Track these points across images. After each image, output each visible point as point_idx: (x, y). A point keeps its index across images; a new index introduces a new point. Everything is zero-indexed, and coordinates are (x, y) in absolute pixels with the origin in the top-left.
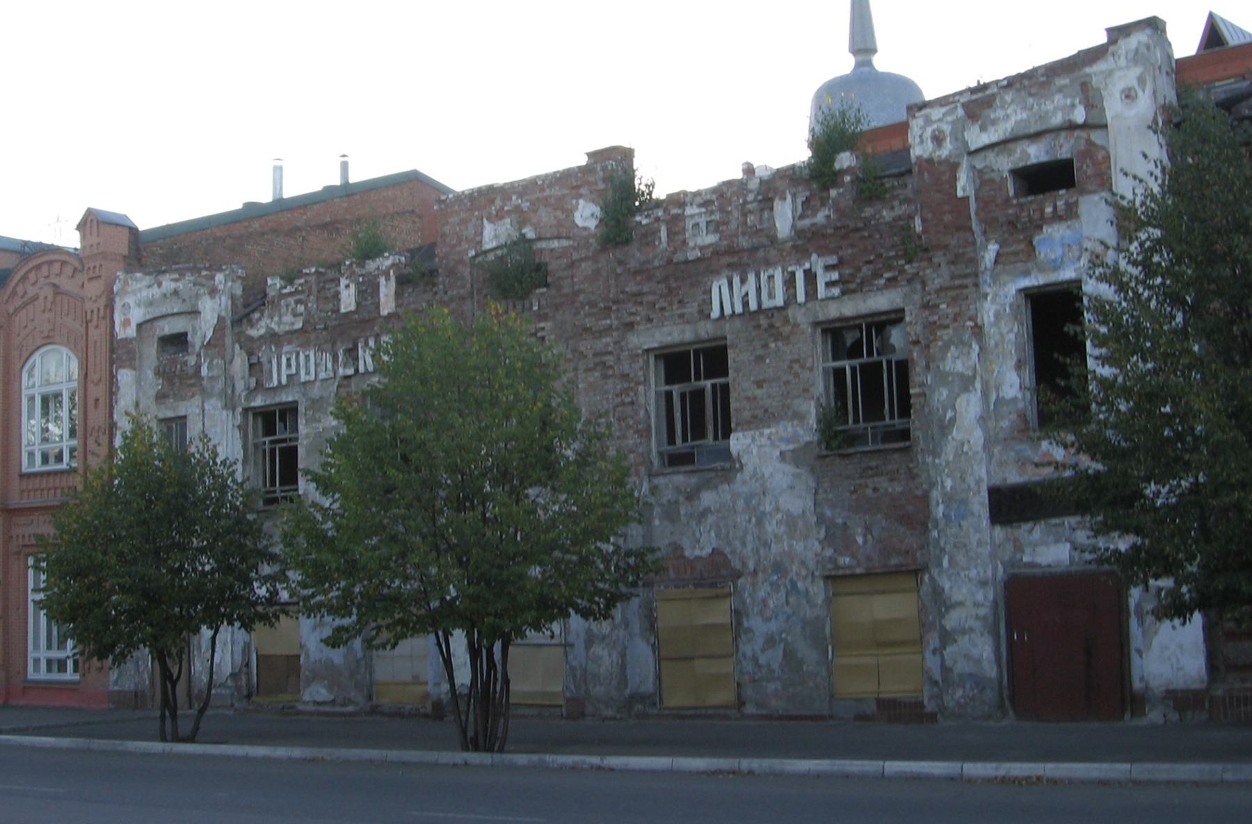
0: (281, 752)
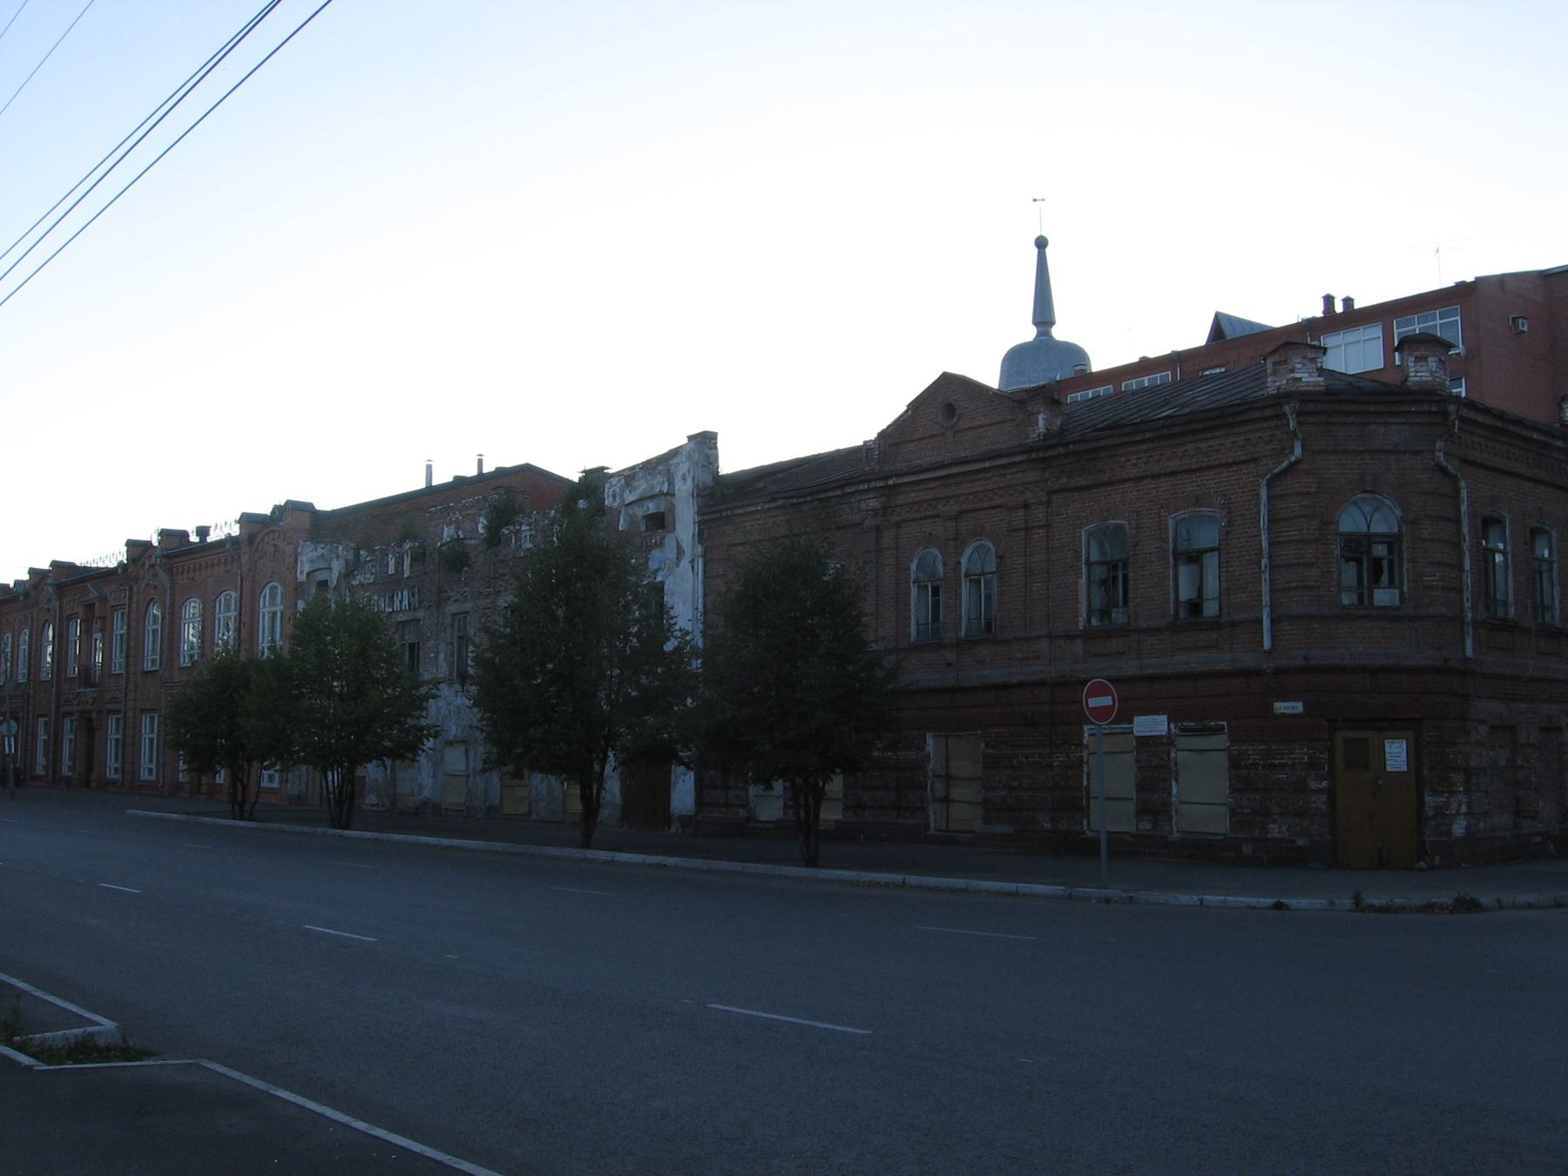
0: (670, 861)
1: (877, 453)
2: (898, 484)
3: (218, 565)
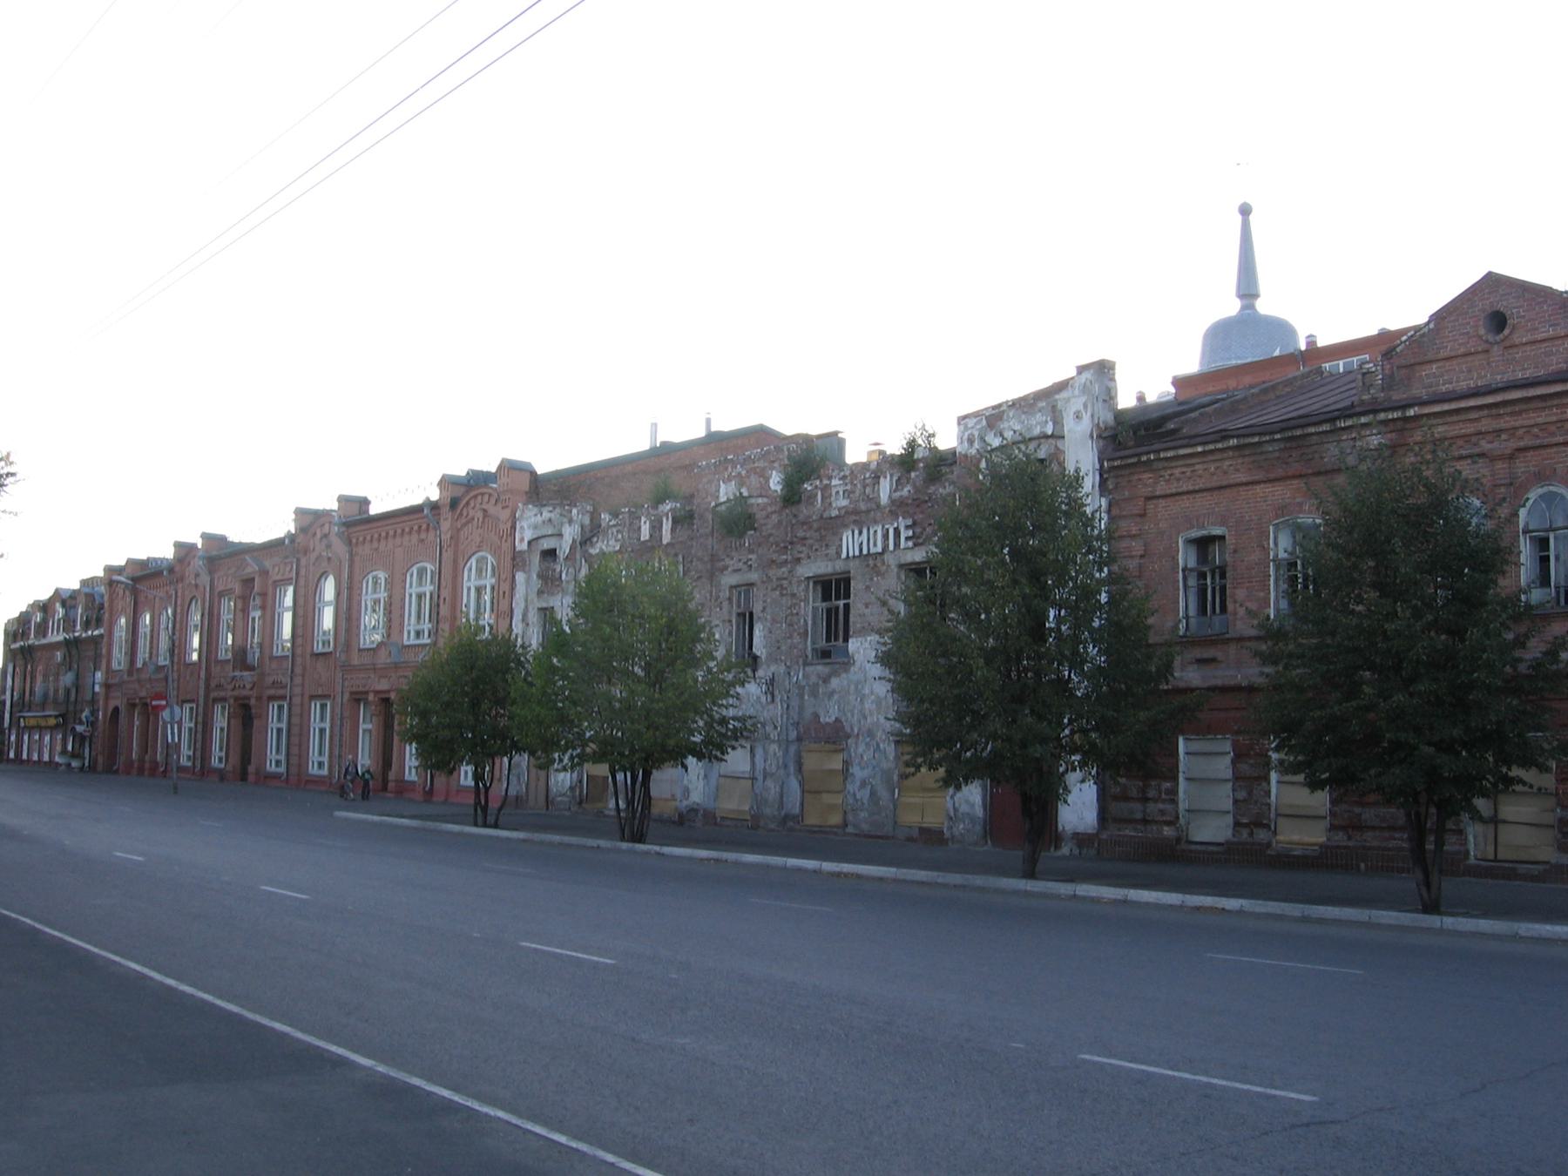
1: (1380, 377)
2: (1422, 416)
3: (410, 533)
